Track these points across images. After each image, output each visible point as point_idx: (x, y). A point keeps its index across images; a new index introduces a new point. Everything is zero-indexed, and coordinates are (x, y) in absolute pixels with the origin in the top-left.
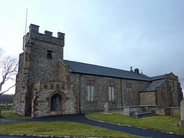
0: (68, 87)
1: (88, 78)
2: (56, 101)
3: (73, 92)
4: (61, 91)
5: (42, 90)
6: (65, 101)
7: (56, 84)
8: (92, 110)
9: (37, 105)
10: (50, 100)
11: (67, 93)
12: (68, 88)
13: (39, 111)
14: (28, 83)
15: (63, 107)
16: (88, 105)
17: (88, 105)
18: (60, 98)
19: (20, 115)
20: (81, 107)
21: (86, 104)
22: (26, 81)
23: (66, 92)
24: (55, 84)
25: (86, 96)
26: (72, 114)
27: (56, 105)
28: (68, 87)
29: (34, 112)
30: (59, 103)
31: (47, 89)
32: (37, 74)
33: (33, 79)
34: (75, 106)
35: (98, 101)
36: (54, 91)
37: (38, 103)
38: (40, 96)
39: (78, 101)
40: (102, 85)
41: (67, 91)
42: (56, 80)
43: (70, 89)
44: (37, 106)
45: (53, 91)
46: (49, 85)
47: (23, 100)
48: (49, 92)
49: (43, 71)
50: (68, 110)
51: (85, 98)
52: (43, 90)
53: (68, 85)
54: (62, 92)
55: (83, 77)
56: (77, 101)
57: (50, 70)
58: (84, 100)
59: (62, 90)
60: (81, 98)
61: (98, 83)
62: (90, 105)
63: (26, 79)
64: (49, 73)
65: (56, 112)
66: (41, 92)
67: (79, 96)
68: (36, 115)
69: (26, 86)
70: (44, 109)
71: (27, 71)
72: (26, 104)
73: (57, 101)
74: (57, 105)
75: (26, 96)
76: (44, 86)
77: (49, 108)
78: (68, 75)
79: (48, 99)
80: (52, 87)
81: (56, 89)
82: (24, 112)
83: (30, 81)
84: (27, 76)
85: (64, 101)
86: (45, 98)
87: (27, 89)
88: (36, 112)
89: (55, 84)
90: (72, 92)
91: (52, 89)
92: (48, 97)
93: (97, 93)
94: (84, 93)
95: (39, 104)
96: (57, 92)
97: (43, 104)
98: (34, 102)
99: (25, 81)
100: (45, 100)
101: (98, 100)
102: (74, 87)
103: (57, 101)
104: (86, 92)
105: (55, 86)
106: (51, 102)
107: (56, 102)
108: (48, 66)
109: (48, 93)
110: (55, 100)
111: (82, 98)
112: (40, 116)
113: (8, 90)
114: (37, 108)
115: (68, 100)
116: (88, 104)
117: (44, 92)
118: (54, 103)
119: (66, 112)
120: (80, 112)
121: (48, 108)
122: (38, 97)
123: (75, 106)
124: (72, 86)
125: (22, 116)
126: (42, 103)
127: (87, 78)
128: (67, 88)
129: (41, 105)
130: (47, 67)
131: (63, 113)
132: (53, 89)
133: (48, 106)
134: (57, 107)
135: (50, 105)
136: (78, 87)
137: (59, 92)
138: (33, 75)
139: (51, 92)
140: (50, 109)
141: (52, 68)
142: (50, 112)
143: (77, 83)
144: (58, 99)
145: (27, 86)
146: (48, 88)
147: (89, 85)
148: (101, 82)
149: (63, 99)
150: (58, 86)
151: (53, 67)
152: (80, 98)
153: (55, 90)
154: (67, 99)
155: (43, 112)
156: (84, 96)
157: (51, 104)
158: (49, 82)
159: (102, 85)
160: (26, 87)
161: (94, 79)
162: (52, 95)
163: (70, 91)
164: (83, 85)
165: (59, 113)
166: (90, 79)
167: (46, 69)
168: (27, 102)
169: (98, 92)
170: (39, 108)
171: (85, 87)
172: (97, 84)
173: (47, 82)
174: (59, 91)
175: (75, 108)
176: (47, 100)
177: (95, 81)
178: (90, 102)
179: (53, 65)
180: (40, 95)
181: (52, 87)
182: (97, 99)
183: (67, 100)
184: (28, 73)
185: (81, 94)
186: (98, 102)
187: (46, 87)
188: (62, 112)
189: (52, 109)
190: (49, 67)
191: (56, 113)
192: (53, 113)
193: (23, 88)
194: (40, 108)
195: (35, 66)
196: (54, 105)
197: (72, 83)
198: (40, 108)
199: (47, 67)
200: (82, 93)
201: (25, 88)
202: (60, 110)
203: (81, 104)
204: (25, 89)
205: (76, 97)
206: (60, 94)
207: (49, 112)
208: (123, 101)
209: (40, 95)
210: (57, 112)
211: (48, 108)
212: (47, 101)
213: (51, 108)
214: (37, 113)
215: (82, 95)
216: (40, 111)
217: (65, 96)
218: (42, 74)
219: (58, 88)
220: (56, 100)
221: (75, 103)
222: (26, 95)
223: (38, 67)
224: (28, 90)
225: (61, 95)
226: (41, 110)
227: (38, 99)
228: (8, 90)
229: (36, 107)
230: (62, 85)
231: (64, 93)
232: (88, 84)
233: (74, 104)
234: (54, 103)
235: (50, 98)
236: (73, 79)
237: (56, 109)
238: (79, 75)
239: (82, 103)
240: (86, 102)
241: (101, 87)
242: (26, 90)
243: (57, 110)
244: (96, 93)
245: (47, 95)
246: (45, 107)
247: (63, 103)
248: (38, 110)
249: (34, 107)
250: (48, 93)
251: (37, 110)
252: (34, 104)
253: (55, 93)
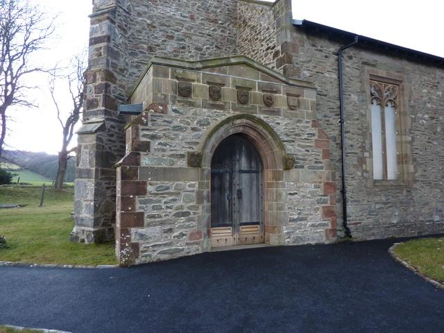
0: (293, 102)
1: (374, 66)
2: (237, 176)
3: (315, 131)
4: (260, 122)
5: (165, 107)
6: (277, 177)
7: (234, 81)
8: (395, 222)
9: (141, 190)
10: (207, 166)
11: (287, 135)
12: (291, 108)
13: (149, 225)
14: (107, 86)
15: (270, 205)
16: (377, 199)
17: (377, 199)
18: (255, 156)
19: (77, 238)
20: (350, 209)
21: (369, 194)
22: (98, 76)
23: (281, 124)
24: (231, 78)
25: (366, 154)
26: (313, 243)
27: (235, 196)
28: (293, 102)
29: (125, 231)
30: (251, 179)
31: (192, 104)
32: (151, 49)
33: (131, 70)
34: (325, 202)
35: (416, 181)
36: (228, 120)
37: (145, 183)
38: (155, 145)
39: (338, 175)
40: (429, 105)
41: (287, 121)
42: (233, 61)
43: (297, 111)
44: (137, 199)
45: (223, 116)
46: (199, 84)
47: (88, 167)
48: (200, 123)
49: (172, 37)
50: (293, 225)
51: (365, 163)
52: (170, 107)
53: (294, 91)
54: (265, 125)
55: (350, 58)
56: (334, 178)
57: (202, 35)
58: (359, 174)
59: (262, 117)
60: (347, 160)
61: (411, 93)
62: (384, 199)
63: (101, 66)
64: (200, 49)
65: (168, 103)
66: (159, 121)
67: (337, 154)
68: (135, 247)
69: (100, 97)
70: (177, 215)
71: (105, 28)
72: (97, 184)
73: (241, 172)
74: (240, 192)
75: (98, 146)
76: (172, 84)
77: (203, 212)
78: (289, 40)
79: (195, 160)
80: (215, 93)
81: (235, 110)
82: (91, 223)
83: (115, 74)
84: (102, 51)
85: (274, 172)
86: (182, 156)
87: (106, 113)
88: (133, 230)
89: (231, 80)
90: (308, 131)
91: (213, 106)
92: (196, 149)
93: (411, 143)
94: (360, 139)
95: (150, 188)
96: (238, 121)
97: (172, 185)
98: (124, 177)
99: (95, 76)
100: (182, 163)
101: (417, 174)
102: (317, 106)
103: (241, 172)
104: (365, 133)
105: (229, 90)
106: (213, 175)
107: (236, 181)
108: (192, 18)
109: (194, 129)
110: (232, 169)
111: (350, 161)
112: (155, 256)
113: (58, 117)
114: (138, 208)
115: (293, 172)
116: (376, 194)
117: (176, 123)
118: (227, 185)
119: (285, 236)
120: (348, 232)
121: (200, 211)
122: (146, 147)
123: (325, 202)
124: (309, 97)
125: (83, 241)
126: (167, 183)
127: (367, 68)
128: (286, 108)
129: (162, 191)
130: (189, 23)
131: (274, 241)
132: (221, 107)
133: (200, 199)
134: (240, 204)
135: (207, 191)
136: (332, 105)
137: (254, 129)
138: (133, 54)
139: (213, 124)
140: (208, 215)
141: (209, 28)
142: (209, 234)
143: (328, 87)
144: (243, 163)
145: (106, 98)
146: (193, 99)
147: (375, 102)
148: (425, 91)
149: (268, 160)
150: (243, 95)
151: (215, 21)
152: (342, 160)
153: (231, 113)
154: (289, 163)
155: (170, 230)
156: (358, 151)
157: (213, 189)
158: (199, 65)
159: (429, 105)
160: (101, 104)
161: (394, 75)
162: (214, 142)
163: (299, 121)
164: (354, 97)
165: (248, 236)
166: (382, 73)
167: (184, 30)
168: (103, 172)
169: (413, 139)
170: (149, 211)
171: (362, 111)
172: (409, 101)
173: (187, 65)
174: (252, 118)
175: (328, 213)
176: (191, 164)
177: (397, 82)
178: (382, 185)
179: (212, 16)
180: (154, 137)
181: (215, 93)
182: (412, 169)
183: (287, 168)
184: (108, 38)
185: (347, 142)
186: (415, 186)
187: (184, 92)
188: (264, 230)
189: (220, 215)
190: (198, 22)
191: (236, 236)
192: (224, 238)
193: (88, 108)
194: (154, 208)
195: (139, 14)
196: (227, 193)
197: (308, 85)
198: (155, 212)
199: (189, 23)
200: (351, 141)
201: (97, 105)
202: (255, 220)
203: (348, 195)
204: (95, 114)
205: (327, 154)
206: (252, 134)
207: (204, 231)
208: (337, 164)
209: (154, 137)
210: (244, 229)
211: (200, 211)
212: (193, 172)
213: (213, 207)
214: (142, 236)
215: (352, 146)
216: (158, 228)
217: (277, 149)
218: (169, 49)
219: (245, 103)
220: (237, 167)
221: (327, 184)
222: (98, 139)
223: (150, 18)
224: (107, 119)
225: (261, 145)
226: (162, 223)
227: (145, 161)
228: (58, 117)
229: (132, 203)
230: (262, 88)
231: (272, 132)
232: (372, 95)
233: (320, 192)
234: (227, 185)
235: (208, 154)
236: (311, 65)
237: (235, 216)
238: (333, 48)
239: (351, 184)
240: (370, 184)
241: (426, 116)
242: (101, 118)
243: (240, 217)
244: (406, 142)
245: (190, 136)
246: (180, 203)
247: (270, 185)
248: (147, 220)
249: (127, 202)
250: (194, 129)
251: (139, 220)
252: (123, 185)
253: (232, 131)
